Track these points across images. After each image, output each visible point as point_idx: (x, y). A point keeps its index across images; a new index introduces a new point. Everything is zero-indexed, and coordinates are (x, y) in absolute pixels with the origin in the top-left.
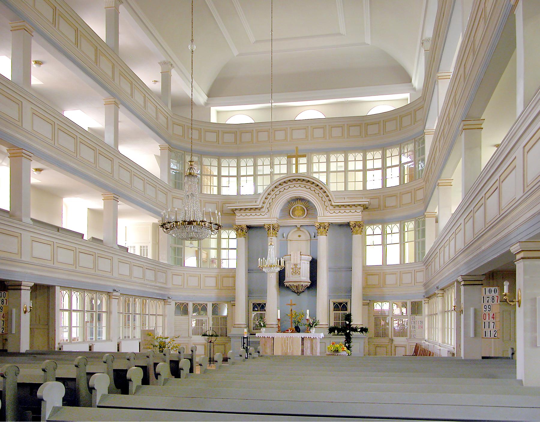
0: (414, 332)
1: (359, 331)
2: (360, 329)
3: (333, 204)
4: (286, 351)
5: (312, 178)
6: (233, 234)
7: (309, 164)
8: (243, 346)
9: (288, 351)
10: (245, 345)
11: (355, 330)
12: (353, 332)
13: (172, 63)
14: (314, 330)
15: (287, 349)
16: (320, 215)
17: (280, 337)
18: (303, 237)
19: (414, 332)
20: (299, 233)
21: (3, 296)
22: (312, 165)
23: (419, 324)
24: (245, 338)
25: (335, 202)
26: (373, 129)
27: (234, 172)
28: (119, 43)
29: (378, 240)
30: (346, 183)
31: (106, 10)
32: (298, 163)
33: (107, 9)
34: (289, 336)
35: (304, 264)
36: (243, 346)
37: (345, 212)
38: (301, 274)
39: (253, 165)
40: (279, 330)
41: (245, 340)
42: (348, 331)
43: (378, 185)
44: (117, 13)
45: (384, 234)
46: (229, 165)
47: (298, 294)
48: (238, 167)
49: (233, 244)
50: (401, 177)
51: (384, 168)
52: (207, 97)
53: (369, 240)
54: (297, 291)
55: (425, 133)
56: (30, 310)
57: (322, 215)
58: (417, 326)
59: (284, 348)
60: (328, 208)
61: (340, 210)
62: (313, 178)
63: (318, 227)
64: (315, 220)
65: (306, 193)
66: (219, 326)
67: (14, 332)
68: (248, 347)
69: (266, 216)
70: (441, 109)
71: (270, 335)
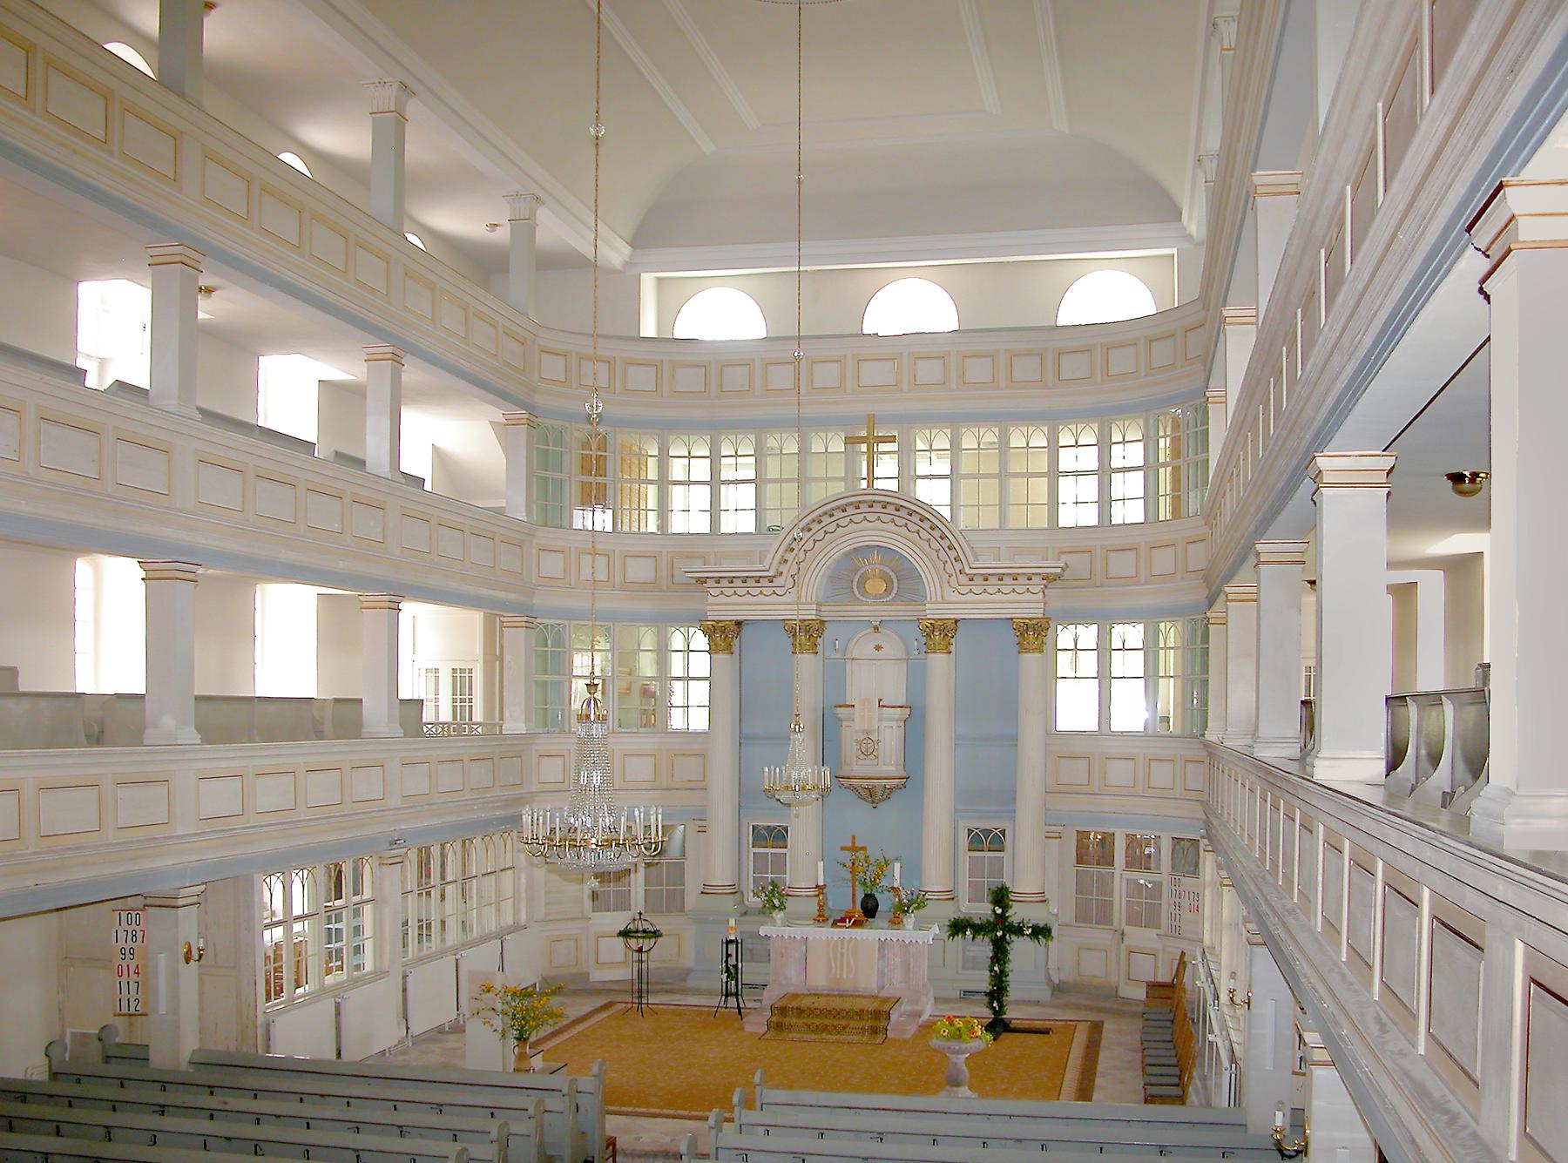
0: (1178, 920)
1: (1028, 935)
2: (1030, 930)
3: (968, 571)
4: (838, 976)
5: (912, 501)
6: (700, 641)
7: (906, 458)
8: (727, 962)
9: (845, 976)
10: (732, 961)
11: (1019, 931)
12: (1013, 937)
13: (540, 193)
14: (913, 919)
15: (842, 970)
16: (934, 599)
17: (824, 938)
18: (887, 651)
19: (1178, 920)
20: (878, 639)
21: (134, 922)
22: (912, 485)
23: (1192, 898)
24: (731, 941)
25: (974, 566)
26: (1073, 366)
27: (701, 470)
28: (406, 159)
29: (1089, 663)
30: (1003, 505)
31: (373, 118)
32: (875, 450)
33: (373, 115)
34: (847, 938)
35: (888, 730)
36: (727, 962)
37: (999, 591)
38: (881, 758)
39: (753, 453)
40: (819, 916)
41: (732, 948)
42: (999, 934)
43: (1088, 516)
44: (401, 118)
45: (1104, 650)
46: (689, 453)
47: (875, 805)
48: (715, 458)
49: (701, 664)
50: (1150, 497)
51: (1105, 472)
52: (630, 248)
53: (1064, 662)
54: (872, 795)
55: (1225, 322)
56: (200, 956)
57: (939, 599)
58: (1185, 904)
59: (834, 970)
60: (953, 580)
61: (985, 587)
62: (915, 502)
63: (927, 630)
64: (921, 608)
65: (895, 536)
66: (662, 890)
67: (163, 1010)
68: (740, 965)
69: (787, 598)
70: (1234, 404)
71: (797, 932)
